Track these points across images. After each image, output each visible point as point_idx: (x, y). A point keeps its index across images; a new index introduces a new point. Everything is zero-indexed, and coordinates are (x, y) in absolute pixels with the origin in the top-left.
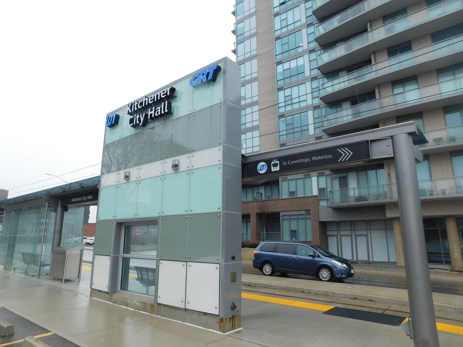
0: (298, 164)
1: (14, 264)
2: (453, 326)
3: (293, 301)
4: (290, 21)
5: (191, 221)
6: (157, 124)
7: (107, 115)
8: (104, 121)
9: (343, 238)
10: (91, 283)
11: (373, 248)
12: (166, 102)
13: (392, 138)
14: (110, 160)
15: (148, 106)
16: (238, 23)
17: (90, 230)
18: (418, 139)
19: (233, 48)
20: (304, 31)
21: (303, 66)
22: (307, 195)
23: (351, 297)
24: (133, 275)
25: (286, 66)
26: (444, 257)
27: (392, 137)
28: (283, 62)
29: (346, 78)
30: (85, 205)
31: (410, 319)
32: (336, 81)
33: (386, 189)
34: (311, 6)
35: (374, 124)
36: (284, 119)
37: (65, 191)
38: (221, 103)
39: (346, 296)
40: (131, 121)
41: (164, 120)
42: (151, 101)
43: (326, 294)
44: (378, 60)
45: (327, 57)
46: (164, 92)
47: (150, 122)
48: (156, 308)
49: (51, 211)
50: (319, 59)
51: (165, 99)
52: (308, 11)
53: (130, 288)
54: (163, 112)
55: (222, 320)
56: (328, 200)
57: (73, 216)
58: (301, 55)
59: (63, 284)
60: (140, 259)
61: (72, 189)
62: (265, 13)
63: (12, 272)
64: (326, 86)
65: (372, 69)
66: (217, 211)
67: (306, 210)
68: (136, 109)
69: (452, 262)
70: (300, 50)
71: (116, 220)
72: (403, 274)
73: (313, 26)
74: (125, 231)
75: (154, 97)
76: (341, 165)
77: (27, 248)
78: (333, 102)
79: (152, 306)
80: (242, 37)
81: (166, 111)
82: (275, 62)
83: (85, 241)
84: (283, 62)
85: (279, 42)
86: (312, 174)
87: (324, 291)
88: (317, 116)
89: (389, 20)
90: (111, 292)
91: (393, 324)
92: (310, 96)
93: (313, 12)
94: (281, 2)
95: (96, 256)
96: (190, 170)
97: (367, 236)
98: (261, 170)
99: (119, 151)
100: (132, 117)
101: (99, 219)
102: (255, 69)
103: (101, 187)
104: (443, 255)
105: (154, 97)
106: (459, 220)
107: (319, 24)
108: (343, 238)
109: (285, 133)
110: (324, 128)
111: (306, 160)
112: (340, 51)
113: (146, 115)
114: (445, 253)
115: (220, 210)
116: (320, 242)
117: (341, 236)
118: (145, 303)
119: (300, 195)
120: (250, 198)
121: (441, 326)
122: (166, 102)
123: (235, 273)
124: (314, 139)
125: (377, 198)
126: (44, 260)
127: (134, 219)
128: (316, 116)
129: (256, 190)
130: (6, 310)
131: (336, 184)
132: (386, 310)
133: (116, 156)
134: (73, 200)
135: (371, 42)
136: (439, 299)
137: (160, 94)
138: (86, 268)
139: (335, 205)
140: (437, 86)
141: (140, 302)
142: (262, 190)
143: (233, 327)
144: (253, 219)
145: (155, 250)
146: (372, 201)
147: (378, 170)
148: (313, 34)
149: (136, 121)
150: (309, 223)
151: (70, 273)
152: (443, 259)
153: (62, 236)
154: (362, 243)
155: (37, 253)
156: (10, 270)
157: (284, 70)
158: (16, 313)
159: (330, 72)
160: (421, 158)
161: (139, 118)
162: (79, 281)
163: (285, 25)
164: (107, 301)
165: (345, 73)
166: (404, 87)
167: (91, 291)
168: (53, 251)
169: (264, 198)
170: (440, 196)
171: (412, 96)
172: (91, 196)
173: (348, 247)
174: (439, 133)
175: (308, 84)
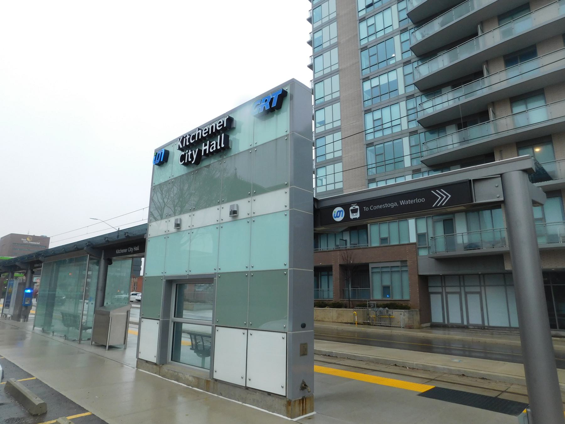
1: (53, 326)
4: (379, 27)
5: (251, 280)
6: (213, 161)
7: (156, 150)
8: (152, 157)
9: (449, 296)
11: (495, 309)
13: (501, 177)
14: (164, 201)
16: (315, 31)
19: (309, 62)
20: (397, 39)
21: (396, 82)
22: (402, 243)
23: (458, 373)
24: (186, 341)
25: (375, 82)
28: (370, 78)
29: (450, 96)
31: (529, 410)
32: (438, 100)
34: (405, 7)
35: (486, 154)
36: (373, 148)
38: (287, 135)
39: (450, 372)
40: (183, 158)
41: (221, 156)
42: (205, 134)
43: (425, 369)
44: (492, 72)
45: (426, 70)
47: (205, 159)
48: (212, 385)
49: (94, 263)
50: (415, 73)
53: (182, 358)
54: (219, 147)
56: (429, 248)
57: (120, 269)
58: (394, 68)
59: (107, 351)
60: (196, 320)
62: (349, 19)
63: (51, 335)
65: (484, 83)
66: (283, 267)
67: (401, 261)
70: (392, 62)
71: (165, 277)
73: (408, 32)
74: (179, 290)
77: (68, 308)
78: (435, 125)
79: (208, 382)
80: (320, 48)
81: (223, 146)
82: (361, 78)
84: (370, 78)
85: (365, 53)
87: (422, 365)
88: (414, 144)
92: (404, 120)
93: (407, 14)
94: (367, 4)
95: (143, 320)
96: (251, 217)
97: (480, 293)
99: (175, 190)
100: (183, 153)
102: (336, 87)
103: (149, 237)
107: (416, 29)
108: (449, 296)
110: (423, 159)
111: (393, 205)
112: (442, 62)
113: (200, 151)
115: (287, 267)
116: (420, 301)
117: (447, 293)
118: (198, 378)
119: (394, 242)
120: (332, 246)
123: (306, 344)
125: (493, 245)
126: (86, 322)
127: (186, 276)
131: (440, 228)
132: (503, 392)
133: (164, 199)
134: (118, 252)
135: (482, 48)
137: (216, 125)
138: (133, 331)
139: (438, 255)
141: (194, 377)
143: (304, 412)
144: (336, 271)
146: (486, 249)
147: (493, 211)
148: (408, 42)
150: (406, 277)
151: (114, 338)
154: (473, 302)
156: (48, 333)
157: (372, 88)
158: (51, 387)
161: (192, 155)
162: (125, 349)
164: (156, 373)
165: (449, 88)
167: (137, 361)
168: (95, 312)
169: (348, 246)
171: (537, 115)
175: (403, 104)
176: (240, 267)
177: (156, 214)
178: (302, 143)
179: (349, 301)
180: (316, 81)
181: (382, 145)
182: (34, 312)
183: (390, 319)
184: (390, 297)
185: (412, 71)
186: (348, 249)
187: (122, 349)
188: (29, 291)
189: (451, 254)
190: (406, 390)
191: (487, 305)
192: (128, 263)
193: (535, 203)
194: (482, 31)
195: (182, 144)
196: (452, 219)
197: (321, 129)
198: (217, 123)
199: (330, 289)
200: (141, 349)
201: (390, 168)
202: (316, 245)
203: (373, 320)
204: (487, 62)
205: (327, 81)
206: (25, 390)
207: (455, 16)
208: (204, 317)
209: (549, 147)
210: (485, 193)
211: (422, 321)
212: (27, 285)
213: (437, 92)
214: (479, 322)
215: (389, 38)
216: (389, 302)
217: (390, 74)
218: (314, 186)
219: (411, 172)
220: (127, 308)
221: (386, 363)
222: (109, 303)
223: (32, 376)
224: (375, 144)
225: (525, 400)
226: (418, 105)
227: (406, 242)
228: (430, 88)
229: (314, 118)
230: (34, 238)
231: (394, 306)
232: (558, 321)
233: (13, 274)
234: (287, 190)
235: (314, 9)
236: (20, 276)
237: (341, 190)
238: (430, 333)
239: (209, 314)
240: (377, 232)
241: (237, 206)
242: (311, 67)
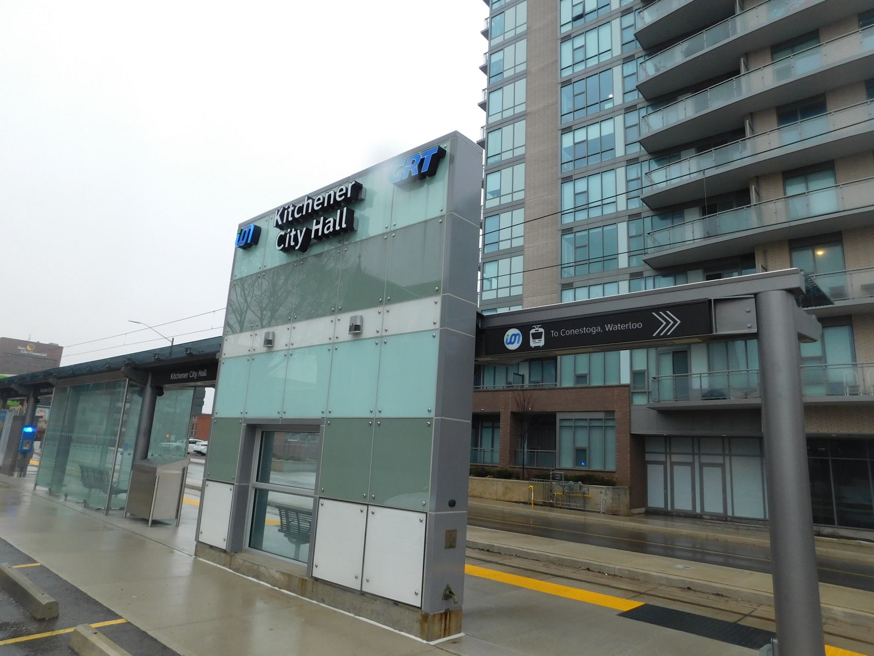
4: (592, 51)
7: (240, 225)
8: (234, 237)
9: (676, 468)
10: (198, 532)
11: (736, 490)
12: (345, 209)
13: (755, 297)
14: (246, 301)
16: (492, 52)
17: (201, 425)
19: (481, 98)
20: (617, 70)
21: (613, 136)
22: (608, 383)
24: (272, 518)
25: (580, 135)
28: (574, 128)
35: (739, 257)
36: (572, 236)
37: (158, 360)
38: (441, 217)
39: (670, 583)
40: (281, 240)
41: (340, 241)
42: (318, 205)
43: (633, 577)
44: (759, 130)
45: (659, 121)
47: (314, 244)
48: (309, 586)
49: (134, 392)
50: (643, 124)
52: (626, 32)
53: (266, 543)
54: (338, 228)
57: (174, 403)
60: (290, 486)
61: (174, 356)
63: (62, 500)
65: (745, 147)
66: (427, 415)
67: (606, 412)
68: (290, 219)
70: (608, 106)
71: (246, 419)
73: (634, 62)
74: (265, 441)
75: (324, 199)
78: (668, 207)
79: (303, 581)
80: (499, 78)
81: (344, 226)
82: (560, 127)
83: (193, 448)
84: (574, 128)
85: (568, 89)
90: (232, 551)
95: (208, 482)
96: (382, 337)
97: (722, 466)
98: (511, 343)
99: (265, 284)
100: (283, 233)
102: (521, 140)
103: (223, 356)
105: (324, 199)
108: (676, 468)
110: (647, 257)
111: (594, 330)
113: (308, 232)
117: (673, 464)
119: (597, 382)
120: (501, 384)
122: (345, 209)
123: (455, 531)
126: (118, 482)
128: (633, 233)
130: (48, 571)
131: (667, 364)
132: (745, 615)
133: (251, 302)
134: (173, 376)
137: (335, 193)
138: (191, 499)
141: (283, 573)
143: (446, 632)
144: (505, 422)
146: (734, 400)
150: (611, 435)
151: (161, 509)
154: (712, 479)
155: (107, 465)
156: (58, 497)
157: (575, 144)
161: (296, 236)
162: (177, 526)
163: (582, 58)
164: (224, 565)
166: (806, 182)
168: (133, 467)
169: (527, 384)
171: (822, 200)
172: (206, 370)
173: (678, 485)
175: (621, 171)
176: (362, 412)
178: (464, 226)
179: (523, 468)
180: (490, 129)
182: (37, 463)
184: (585, 466)
185: (637, 122)
187: (173, 526)
188: (29, 430)
189: (682, 404)
190: (602, 607)
191: (732, 484)
193: (803, 338)
194: (747, 68)
195: (282, 219)
197: (493, 203)
198: (337, 190)
199: (495, 449)
200: (202, 528)
201: (596, 268)
202: (477, 380)
203: (557, 500)
204: (752, 115)
205: (507, 130)
206: (25, 582)
208: (298, 483)
209: (837, 249)
210: (730, 320)
211: (632, 506)
212: (28, 420)
213: (674, 156)
214: (719, 509)
216: (583, 474)
217: (603, 123)
218: (479, 290)
219: (628, 276)
220: (180, 465)
221: (574, 565)
222: (156, 455)
223: (35, 562)
224: (575, 230)
225: (772, 628)
226: (644, 175)
228: (663, 149)
229: (484, 184)
230: (38, 346)
231: (591, 479)
232: (825, 512)
233: (5, 401)
234: (438, 299)
235: (493, 16)
236: (15, 407)
237: (518, 300)
238: (644, 523)
239: (309, 480)
240: (571, 367)
241: (362, 318)
242: (483, 106)
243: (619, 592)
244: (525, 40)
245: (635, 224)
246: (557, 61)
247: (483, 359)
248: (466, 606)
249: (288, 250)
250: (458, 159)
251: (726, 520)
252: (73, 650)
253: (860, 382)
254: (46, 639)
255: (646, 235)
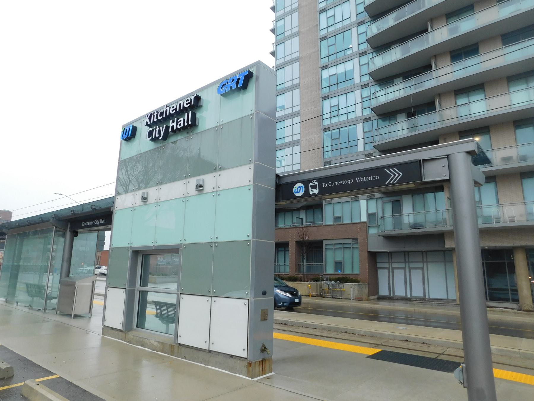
0: (336, 186)
1: (17, 297)
2: (515, 373)
3: (336, 343)
4: (338, 19)
6: (180, 138)
7: (123, 126)
8: (120, 133)
9: (395, 271)
11: (433, 283)
12: (190, 112)
13: (448, 157)
15: (169, 117)
16: (277, 20)
17: (102, 257)
18: (478, 158)
19: (272, 49)
20: (354, 30)
21: (352, 71)
22: (354, 222)
23: (402, 339)
24: (151, 310)
25: (333, 71)
26: (512, 294)
27: (448, 156)
29: (401, 86)
30: (98, 230)
32: (390, 90)
33: (446, 215)
35: (432, 139)
36: (330, 132)
38: (252, 114)
39: (395, 338)
40: (150, 134)
41: (188, 133)
42: (173, 111)
43: (373, 336)
44: (440, 65)
45: (381, 61)
46: (188, 100)
48: (176, 349)
49: (59, 236)
50: (370, 63)
51: (188, 109)
52: (359, 7)
53: (147, 325)
54: (186, 124)
55: (250, 364)
56: (378, 227)
57: (85, 242)
58: (350, 59)
60: (159, 292)
63: (15, 305)
64: (378, 94)
65: (432, 75)
66: (247, 238)
67: (353, 239)
69: (520, 300)
70: (349, 52)
71: (131, 248)
72: (457, 312)
73: (364, 25)
75: (191, 100)
76: (391, 188)
77: (32, 278)
78: (387, 113)
79: (172, 346)
81: (190, 123)
83: (98, 271)
85: (325, 42)
86: (361, 197)
89: (455, 18)
91: (447, 371)
92: (359, 107)
93: (364, 8)
95: (109, 289)
96: (216, 191)
97: (422, 268)
98: (298, 192)
99: (140, 168)
100: (151, 129)
101: (112, 247)
102: (296, 74)
103: (116, 209)
104: (510, 292)
105: (191, 100)
106: (530, 252)
107: (372, 22)
108: (395, 271)
109: (330, 148)
110: (375, 144)
111: (349, 182)
112: (395, 55)
113: (167, 127)
114: (512, 290)
115: (250, 238)
116: (369, 275)
117: (393, 268)
118: (163, 343)
119: (347, 221)
120: (289, 224)
121: (498, 373)
122: (190, 112)
123: (267, 310)
124: (364, 156)
128: (366, 130)
129: (295, 215)
131: (389, 208)
132: (440, 354)
133: (133, 174)
134: (84, 224)
135: (431, 43)
136: (498, 343)
137: (184, 103)
138: (98, 302)
139: (386, 233)
140: (506, 97)
141: (159, 342)
142: (303, 215)
143: (263, 372)
144: (292, 247)
145: (175, 282)
146: (429, 229)
149: (156, 134)
150: (356, 253)
151: (80, 307)
152: (510, 297)
153: (72, 266)
154: (416, 277)
155: (43, 284)
156: (12, 304)
157: (330, 76)
158: (17, 352)
159: (384, 78)
160: (481, 179)
161: (159, 131)
162: (90, 317)
163: (333, 23)
168: (60, 282)
170: (508, 224)
171: (477, 107)
172: (105, 219)
173: (397, 281)
174: (504, 152)
175: (358, 92)
177: (121, 190)
179: (304, 275)
181: (338, 130)
183: (341, 291)
186: (305, 227)
192: (94, 236)
194: (432, 28)
195: (150, 121)
196: (399, 201)
198: (185, 101)
204: (435, 57)
205: (288, 68)
207: (407, 13)
209: (487, 137)
211: (370, 294)
215: (346, 30)
216: (340, 276)
221: (337, 330)
224: (331, 129)
227: (359, 221)
231: (345, 279)
238: (378, 304)
239: (174, 286)
240: (335, 210)
241: (203, 180)
243: (367, 344)
244: (297, 13)
245: (367, 124)
246: (317, 25)
247: (282, 203)
248: (274, 357)
249: (155, 140)
250: (261, 79)
251: (425, 301)
252: (23, 396)
253: (501, 215)
254: (5, 390)
255: (374, 130)
